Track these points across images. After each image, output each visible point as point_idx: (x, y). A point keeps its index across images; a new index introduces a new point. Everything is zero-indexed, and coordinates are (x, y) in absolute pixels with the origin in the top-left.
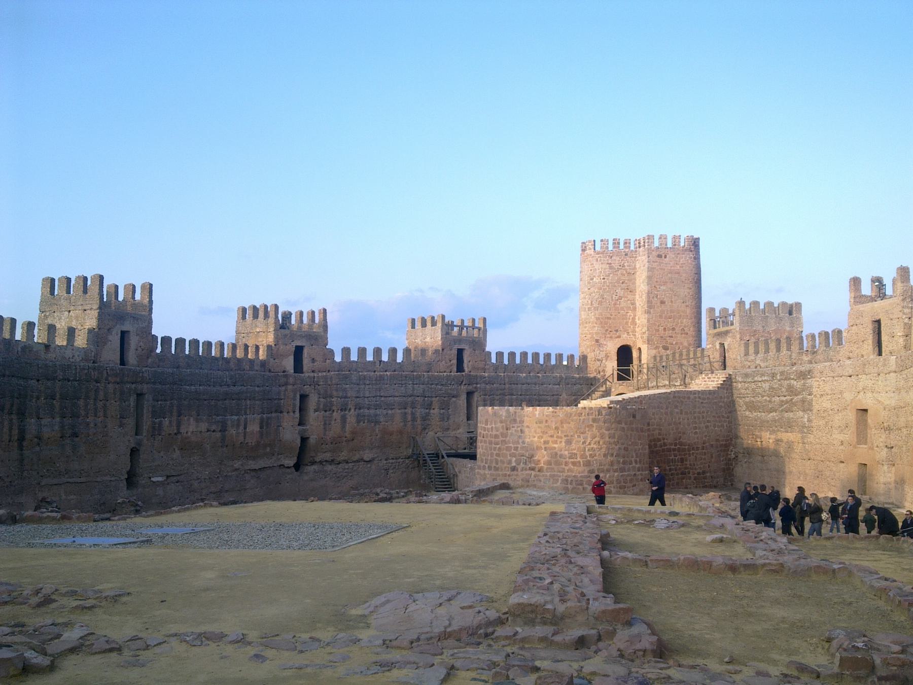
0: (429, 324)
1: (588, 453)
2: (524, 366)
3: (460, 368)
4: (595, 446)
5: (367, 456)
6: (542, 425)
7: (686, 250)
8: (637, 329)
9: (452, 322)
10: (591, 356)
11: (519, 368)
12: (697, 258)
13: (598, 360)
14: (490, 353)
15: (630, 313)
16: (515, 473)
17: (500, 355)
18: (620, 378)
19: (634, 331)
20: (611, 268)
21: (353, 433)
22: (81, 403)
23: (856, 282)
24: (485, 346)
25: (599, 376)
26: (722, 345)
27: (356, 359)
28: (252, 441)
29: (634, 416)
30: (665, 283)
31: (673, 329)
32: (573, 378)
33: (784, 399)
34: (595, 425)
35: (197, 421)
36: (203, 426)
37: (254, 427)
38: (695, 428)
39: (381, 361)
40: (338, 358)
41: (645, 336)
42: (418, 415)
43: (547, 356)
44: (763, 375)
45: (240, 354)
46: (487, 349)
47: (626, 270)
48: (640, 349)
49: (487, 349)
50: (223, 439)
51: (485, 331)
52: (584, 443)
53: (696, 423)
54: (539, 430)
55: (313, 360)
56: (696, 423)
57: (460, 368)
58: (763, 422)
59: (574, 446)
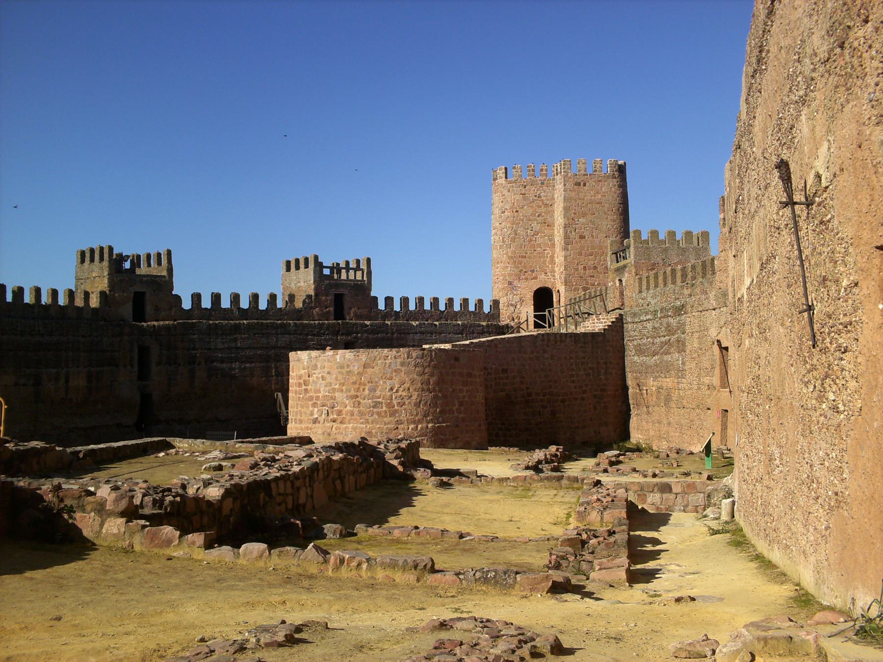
0: (302, 265)
1: (395, 402)
2: (420, 312)
4: (404, 394)
6: (344, 371)
7: (608, 177)
8: (556, 269)
9: (338, 264)
10: (503, 302)
11: (413, 316)
12: (623, 185)
13: (512, 305)
14: (376, 298)
15: (548, 251)
16: (317, 425)
19: (553, 271)
20: (524, 199)
24: (370, 290)
25: (512, 324)
26: (620, 281)
27: (209, 306)
29: (457, 359)
30: (584, 215)
31: (595, 268)
32: (479, 325)
33: (663, 339)
34: (403, 369)
38: (573, 376)
39: (239, 309)
40: (187, 305)
41: (563, 277)
44: (647, 313)
45: (79, 302)
46: (373, 294)
47: (542, 201)
48: (558, 291)
49: (373, 294)
51: (369, 273)
52: (392, 389)
53: (573, 370)
54: (340, 377)
56: (573, 370)
58: (647, 367)
59: (378, 393)
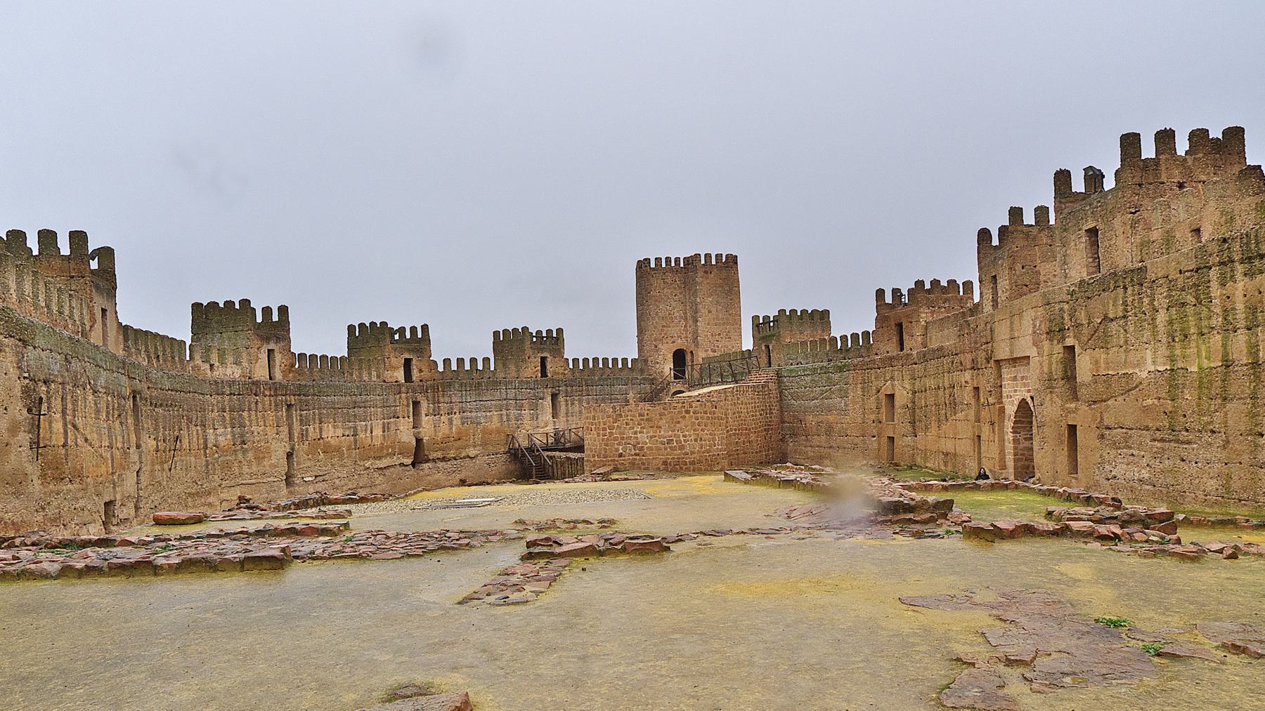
3: (544, 374)
5: (472, 452)
17: (575, 361)
18: (676, 377)
21: (459, 433)
22: (245, 414)
23: (880, 293)
28: (377, 442)
35: (334, 427)
36: (340, 432)
37: (378, 432)
42: (512, 416)
43: (460, 361)
50: (356, 441)
55: (421, 371)
57: (544, 374)
